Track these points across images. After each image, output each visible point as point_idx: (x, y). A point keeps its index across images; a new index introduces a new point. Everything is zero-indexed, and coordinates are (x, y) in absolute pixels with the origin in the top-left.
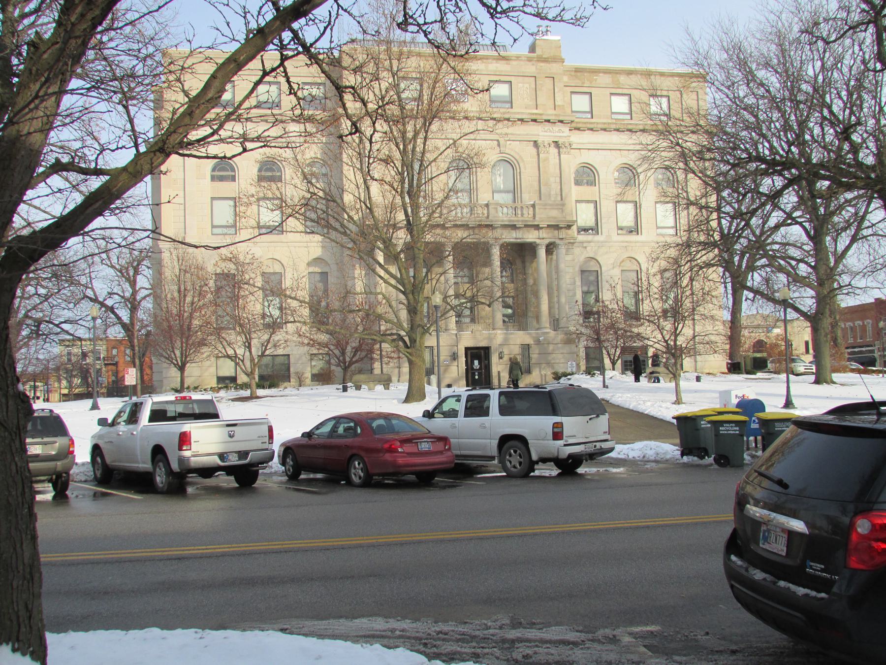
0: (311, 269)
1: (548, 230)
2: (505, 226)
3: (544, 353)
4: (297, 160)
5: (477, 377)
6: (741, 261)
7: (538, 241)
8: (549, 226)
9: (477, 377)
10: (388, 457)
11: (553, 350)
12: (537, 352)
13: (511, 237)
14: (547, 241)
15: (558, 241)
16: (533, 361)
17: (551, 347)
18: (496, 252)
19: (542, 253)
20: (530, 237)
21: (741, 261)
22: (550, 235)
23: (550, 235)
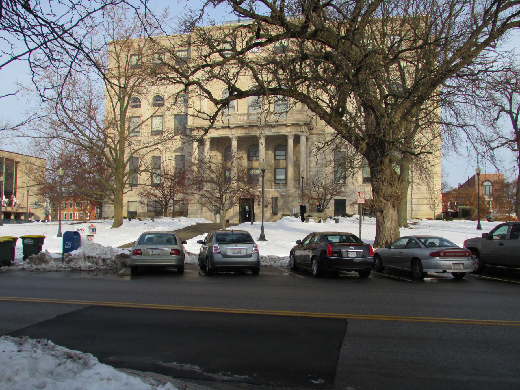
0: (177, 154)
1: (294, 127)
2: (118, 62)
3: (286, 203)
4: (96, 65)
5: (247, 216)
6: (382, 91)
7: (287, 134)
8: (293, 124)
9: (247, 216)
10: (243, 248)
11: (293, 201)
12: (282, 201)
13: (269, 132)
14: (293, 134)
15: (300, 134)
16: (279, 207)
17: (291, 199)
18: (262, 141)
19: (291, 142)
20: (283, 131)
21: (382, 91)
22: (295, 130)
23: (295, 130)
